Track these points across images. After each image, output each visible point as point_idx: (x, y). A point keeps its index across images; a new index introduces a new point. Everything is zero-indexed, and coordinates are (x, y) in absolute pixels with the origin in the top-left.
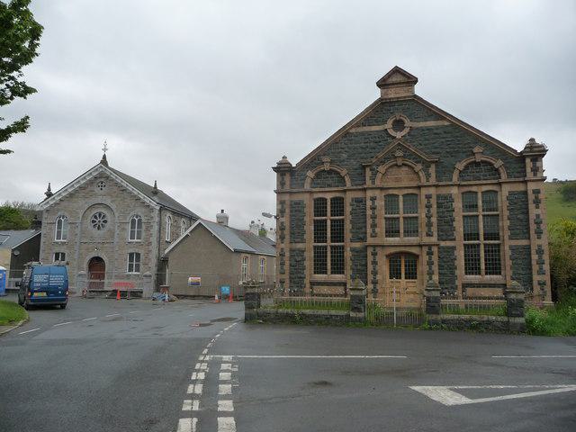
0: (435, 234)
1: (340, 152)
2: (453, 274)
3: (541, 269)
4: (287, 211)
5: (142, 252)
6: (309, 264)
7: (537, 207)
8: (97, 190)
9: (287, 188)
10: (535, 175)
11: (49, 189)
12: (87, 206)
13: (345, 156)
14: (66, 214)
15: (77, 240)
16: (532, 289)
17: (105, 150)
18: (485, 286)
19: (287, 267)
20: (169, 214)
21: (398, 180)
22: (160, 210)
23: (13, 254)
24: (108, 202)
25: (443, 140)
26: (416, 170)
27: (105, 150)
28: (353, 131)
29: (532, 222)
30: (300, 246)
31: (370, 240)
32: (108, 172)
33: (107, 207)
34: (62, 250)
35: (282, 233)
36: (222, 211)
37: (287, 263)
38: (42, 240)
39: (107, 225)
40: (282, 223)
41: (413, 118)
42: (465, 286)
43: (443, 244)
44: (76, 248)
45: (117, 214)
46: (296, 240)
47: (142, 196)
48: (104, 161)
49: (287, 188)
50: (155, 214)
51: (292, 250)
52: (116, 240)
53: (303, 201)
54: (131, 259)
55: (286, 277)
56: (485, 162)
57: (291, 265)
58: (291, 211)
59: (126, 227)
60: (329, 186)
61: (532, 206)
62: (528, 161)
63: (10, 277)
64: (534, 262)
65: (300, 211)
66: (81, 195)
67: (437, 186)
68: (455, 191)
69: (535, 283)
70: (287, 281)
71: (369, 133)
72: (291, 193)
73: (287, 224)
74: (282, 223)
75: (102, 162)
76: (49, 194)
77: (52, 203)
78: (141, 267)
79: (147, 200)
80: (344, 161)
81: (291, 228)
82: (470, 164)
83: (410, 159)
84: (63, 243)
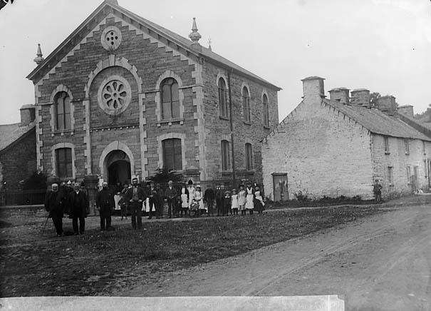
24: (124, 63)
33: (127, 74)
38: (39, 131)
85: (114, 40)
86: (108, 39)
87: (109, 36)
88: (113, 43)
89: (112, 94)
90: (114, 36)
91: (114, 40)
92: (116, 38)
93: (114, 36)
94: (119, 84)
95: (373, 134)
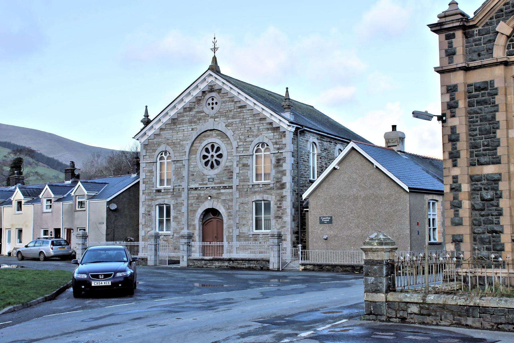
4: (462, 104)
5: (273, 199)
8: (207, 110)
9: (459, 61)
11: (147, 115)
12: (195, 135)
14: (169, 149)
15: (184, 185)
17: (215, 49)
19: (465, 212)
20: (312, 139)
22: (295, 133)
23: (109, 210)
24: (221, 127)
27: (215, 49)
32: (219, 82)
33: (223, 135)
34: (168, 200)
35: (454, 148)
36: (394, 127)
37: (466, 204)
38: (142, 187)
39: (223, 161)
40: (453, 128)
44: (184, 195)
45: (235, 144)
46: (483, 160)
47: (267, 113)
48: (214, 68)
49: (459, 61)
50: (288, 139)
51: (473, 179)
52: (235, 182)
53: (492, 82)
54: (258, 211)
55: (465, 231)
57: (473, 208)
58: (470, 105)
59: (249, 162)
63: (302, 249)
65: (485, 102)
66: (187, 119)
70: (467, 239)
72: (467, 69)
73: (462, 131)
74: (453, 128)
75: (211, 68)
76: (147, 122)
77: (150, 133)
78: (273, 222)
79: (276, 119)
81: (471, 136)
84: (167, 191)
85: (214, 106)
86: (209, 104)
87: (210, 101)
88: (213, 108)
89: (209, 155)
90: (214, 102)
91: (214, 106)
92: (216, 103)
93: (214, 102)
94: (216, 146)
95: (459, 117)
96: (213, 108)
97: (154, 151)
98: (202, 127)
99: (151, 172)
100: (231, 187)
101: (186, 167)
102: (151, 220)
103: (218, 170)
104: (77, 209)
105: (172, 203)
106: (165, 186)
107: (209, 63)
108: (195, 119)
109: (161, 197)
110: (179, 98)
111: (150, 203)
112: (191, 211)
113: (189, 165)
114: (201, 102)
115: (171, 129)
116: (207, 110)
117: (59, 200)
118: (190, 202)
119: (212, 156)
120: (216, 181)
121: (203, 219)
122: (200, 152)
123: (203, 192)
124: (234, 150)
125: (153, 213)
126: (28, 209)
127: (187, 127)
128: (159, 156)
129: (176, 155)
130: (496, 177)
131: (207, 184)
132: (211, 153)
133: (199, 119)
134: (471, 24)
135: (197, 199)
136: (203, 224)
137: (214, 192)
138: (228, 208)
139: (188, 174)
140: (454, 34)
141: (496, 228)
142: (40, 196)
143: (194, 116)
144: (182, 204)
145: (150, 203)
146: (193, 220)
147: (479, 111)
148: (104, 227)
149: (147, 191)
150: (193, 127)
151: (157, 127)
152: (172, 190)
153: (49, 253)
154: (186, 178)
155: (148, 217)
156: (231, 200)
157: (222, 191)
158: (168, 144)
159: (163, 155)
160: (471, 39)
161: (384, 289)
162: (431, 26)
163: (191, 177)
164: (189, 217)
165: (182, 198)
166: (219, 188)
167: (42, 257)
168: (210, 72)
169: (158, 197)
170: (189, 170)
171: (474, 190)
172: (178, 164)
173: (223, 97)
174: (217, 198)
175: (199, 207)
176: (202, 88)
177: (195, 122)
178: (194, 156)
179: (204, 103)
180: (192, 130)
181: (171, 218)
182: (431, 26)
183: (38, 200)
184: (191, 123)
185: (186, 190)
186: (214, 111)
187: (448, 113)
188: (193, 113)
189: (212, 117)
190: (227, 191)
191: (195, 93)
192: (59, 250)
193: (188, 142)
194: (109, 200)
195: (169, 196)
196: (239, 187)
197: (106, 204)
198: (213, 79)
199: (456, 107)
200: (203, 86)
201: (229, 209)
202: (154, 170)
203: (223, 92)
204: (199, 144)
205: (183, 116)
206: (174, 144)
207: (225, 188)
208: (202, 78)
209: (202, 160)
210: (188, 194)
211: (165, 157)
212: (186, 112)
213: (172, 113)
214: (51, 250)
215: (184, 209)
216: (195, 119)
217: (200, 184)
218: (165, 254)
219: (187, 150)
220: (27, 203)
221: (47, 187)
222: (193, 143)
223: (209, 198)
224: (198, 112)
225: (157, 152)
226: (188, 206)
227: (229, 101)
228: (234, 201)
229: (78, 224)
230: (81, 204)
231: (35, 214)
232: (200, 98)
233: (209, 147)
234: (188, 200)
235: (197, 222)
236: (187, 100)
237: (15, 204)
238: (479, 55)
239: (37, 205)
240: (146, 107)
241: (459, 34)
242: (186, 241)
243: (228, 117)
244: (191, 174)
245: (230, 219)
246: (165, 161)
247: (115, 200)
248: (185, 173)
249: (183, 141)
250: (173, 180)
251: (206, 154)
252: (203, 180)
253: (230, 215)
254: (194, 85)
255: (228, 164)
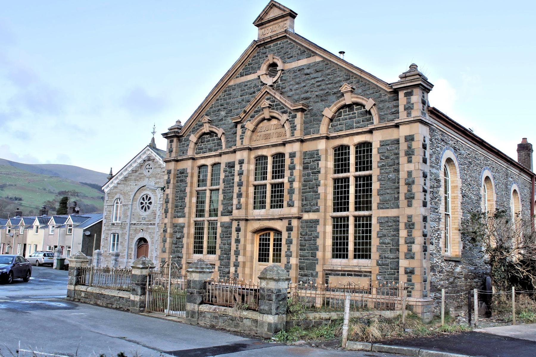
0: (297, 203)
1: (219, 110)
2: (314, 255)
3: (410, 250)
6: (188, 242)
7: (410, 161)
8: (145, 172)
10: (409, 114)
13: (223, 113)
14: (121, 197)
15: (128, 221)
16: (397, 279)
17: (154, 133)
18: (350, 273)
19: (167, 245)
21: (267, 137)
23: (84, 235)
25: (313, 81)
26: (267, 117)
27: (154, 133)
28: (232, 83)
29: (402, 182)
30: (181, 220)
31: (236, 213)
34: (118, 230)
41: (287, 57)
42: (328, 273)
43: (306, 216)
56: (357, 104)
60: (210, 150)
61: (403, 159)
62: (401, 94)
64: (402, 241)
67: (302, 141)
68: (322, 145)
69: (402, 271)
71: (245, 84)
72: (177, 161)
77: (111, 186)
80: (222, 120)
82: (339, 109)
83: (277, 109)
87: (148, 167)
88: (149, 171)
92: (151, 168)
96: (149, 171)
97: (113, 197)
98: (141, 184)
99: (110, 211)
100: (154, 224)
101: (130, 209)
102: (107, 243)
103: (148, 212)
104: (68, 233)
105: (120, 232)
106: (118, 221)
107: (149, 142)
108: (138, 178)
109: (114, 228)
110: (129, 164)
111: (108, 232)
112: (131, 238)
113: (132, 209)
114: (142, 167)
115: (124, 184)
116: (145, 172)
117: (59, 227)
118: (131, 232)
119: (146, 203)
120: (147, 220)
121: (138, 244)
122: (139, 200)
123: (138, 227)
124: (158, 200)
125: (109, 239)
126: (42, 232)
127: (132, 183)
128: (116, 201)
129: (125, 201)
130: (182, 225)
131: (141, 221)
132: (146, 201)
133: (140, 178)
134: (180, 134)
135: (135, 231)
136: (138, 248)
137: (145, 227)
138: (152, 238)
139: (131, 214)
140: (173, 140)
141: (180, 255)
142: (48, 224)
143: (138, 176)
144: (126, 233)
145: (108, 232)
146: (132, 245)
147: (180, 186)
148: (81, 246)
149: (106, 224)
150: (136, 183)
151: (116, 182)
152: (120, 224)
153: (42, 261)
154: (129, 217)
155: (106, 241)
156: (154, 233)
157: (150, 226)
158: (121, 194)
159: (118, 201)
160: (181, 143)
161: (74, 283)
162: (163, 134)
163: (133, 216)
164: (130, 243)
165: (126, 230)
166: (147, 224)
167: (37, 264)
168: (148, 148)
169: (113, 228)
170: (131, 212)
171: (174, 232)
172: (126, 207)
173: (155, 165)
174: (146, 231)
175: (135, 236)
176: (143, 158)
177: (138, 180)
178: (135, 203)
179: (144, 167)
180: (136, 185)
181: (119, 243)
182: (163, 134)
183: (47, 226)
184: (135, 180)
185: (129, 224)
186: (149, 173)
187: (166, 185)
188: (137, 174)
189: (147, 178)
190: (152, 226)
191: (139, 161)
192: (48, 259)
193: (133, 193)
194: (85, 228)
195: (119, 228)
196: (159, 224)
197: (83, 231)
198: (150, 153)
199: (169, 183)
200: (144, 157)
201: (152, 239)
202: (112, 210)
203: (155, 161)
204: (139, 195)
205: (131, 176)
206: (124, 194)
207: (151, 224)
208: (143, 151)
209: (140, 205)
210: (130, 227)
211: (119, 202)
212: (133, 173)
213: (125, 174)
214: (43, 259)
215: (127, 237)
216: (138, 178)
217: (137, 221)
218: (103, 265)
219: (132, 198)
220: (42, 228)
221: (52, 218)
222: (136, 193)
223: (141, 231)
224: (140, 174)
225: (115, 199)
226: (129, 236)
227: (158, 168)
228: (155, 234)
229: (67, 243)
230: (70, 230)
231: (45, 235)
232: (141, 164)
233: (145, 197)
234: (129, 231)
235: (133, 246)
236: (134, 165)
237: (35, 228)
238: (183, 153)
239: (47, 230)
240: (111, 168)
241: (175, 140)
242: (114, 258)
243: (156, 178)
244: (132, 214)
245: (152, 245)
246: (119, 205)
247: (90, 229)
248: (129, 214)
249: (130, 192)
250: (122, 218)
251: (143, 201)
252: (139, 218)
253: (152, 243)
254: (138, 156)
255: (154, 209)
